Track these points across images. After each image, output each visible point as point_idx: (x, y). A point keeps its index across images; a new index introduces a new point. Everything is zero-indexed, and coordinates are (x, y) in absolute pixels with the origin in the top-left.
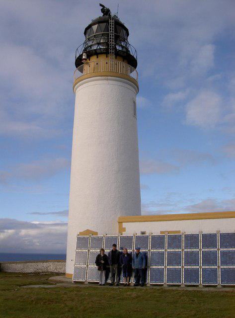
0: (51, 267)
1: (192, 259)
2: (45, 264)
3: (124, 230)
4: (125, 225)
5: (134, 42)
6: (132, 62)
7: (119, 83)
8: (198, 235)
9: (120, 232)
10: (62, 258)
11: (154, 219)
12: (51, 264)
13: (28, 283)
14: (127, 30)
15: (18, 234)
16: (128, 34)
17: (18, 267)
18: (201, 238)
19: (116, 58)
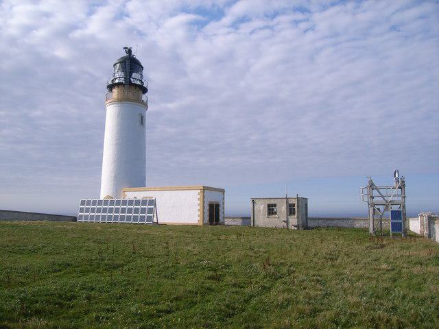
4: (126, 193)
6: (145, 90)
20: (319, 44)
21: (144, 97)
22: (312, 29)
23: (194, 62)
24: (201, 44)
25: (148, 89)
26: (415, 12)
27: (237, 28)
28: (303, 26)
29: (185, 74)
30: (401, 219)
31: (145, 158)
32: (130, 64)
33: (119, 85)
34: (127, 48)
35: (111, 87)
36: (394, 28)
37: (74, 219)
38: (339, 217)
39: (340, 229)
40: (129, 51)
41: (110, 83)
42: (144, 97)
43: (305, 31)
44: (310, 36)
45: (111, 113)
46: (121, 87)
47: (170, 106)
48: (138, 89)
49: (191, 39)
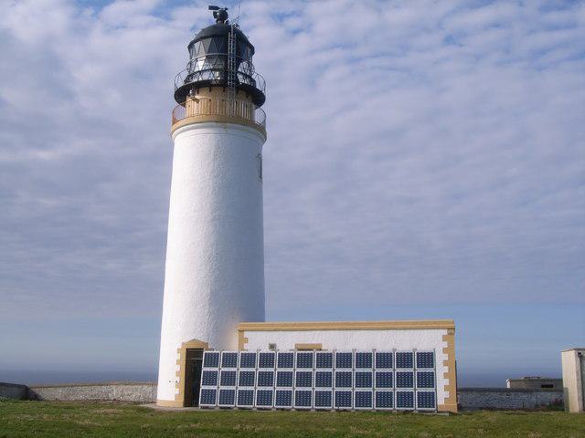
0: (132, 393)
1: (384, 380)
2: (104, 388)
3: (246, 340)
4: (246, 334)
5: (261, 67)
6: (257, 98)
7: (216, 131)
8: (236, 354)
9: (241, 347)
10: (152, 379)
11: (357, 327)
12: (113, 387)
13: (515, 406)
14: (252, 48)
15: (449, 334)
16: (253, 53)
17: (59, 394)
18: (395, 358)
19: (237, 93)
20: (323, 57)
21: (258, 116)
22: (307, 28)
23: (86, 75)
24: (98, 41)
25: (268, 94)
26: (484, 15)
27: (168, 18)
28: (293, 23)
29: (69, 96)
30: (419, 393)
31: (263, 255)
32: (226, 43)
33: (200, 86)
34: (217, 8)
35: (181, 95)
36: (449, 40)
37: (27, 394)
38: (472, 387)
39: (512, 410)
40: (223, 16)
41: (181, 84)
42: (258, 116)
43: (296, 32)
44: (302, 42)
45: (191, 153)
46: (218, 91)
47: (44, 155)
48: (242, 94)
49: (79, 31)
